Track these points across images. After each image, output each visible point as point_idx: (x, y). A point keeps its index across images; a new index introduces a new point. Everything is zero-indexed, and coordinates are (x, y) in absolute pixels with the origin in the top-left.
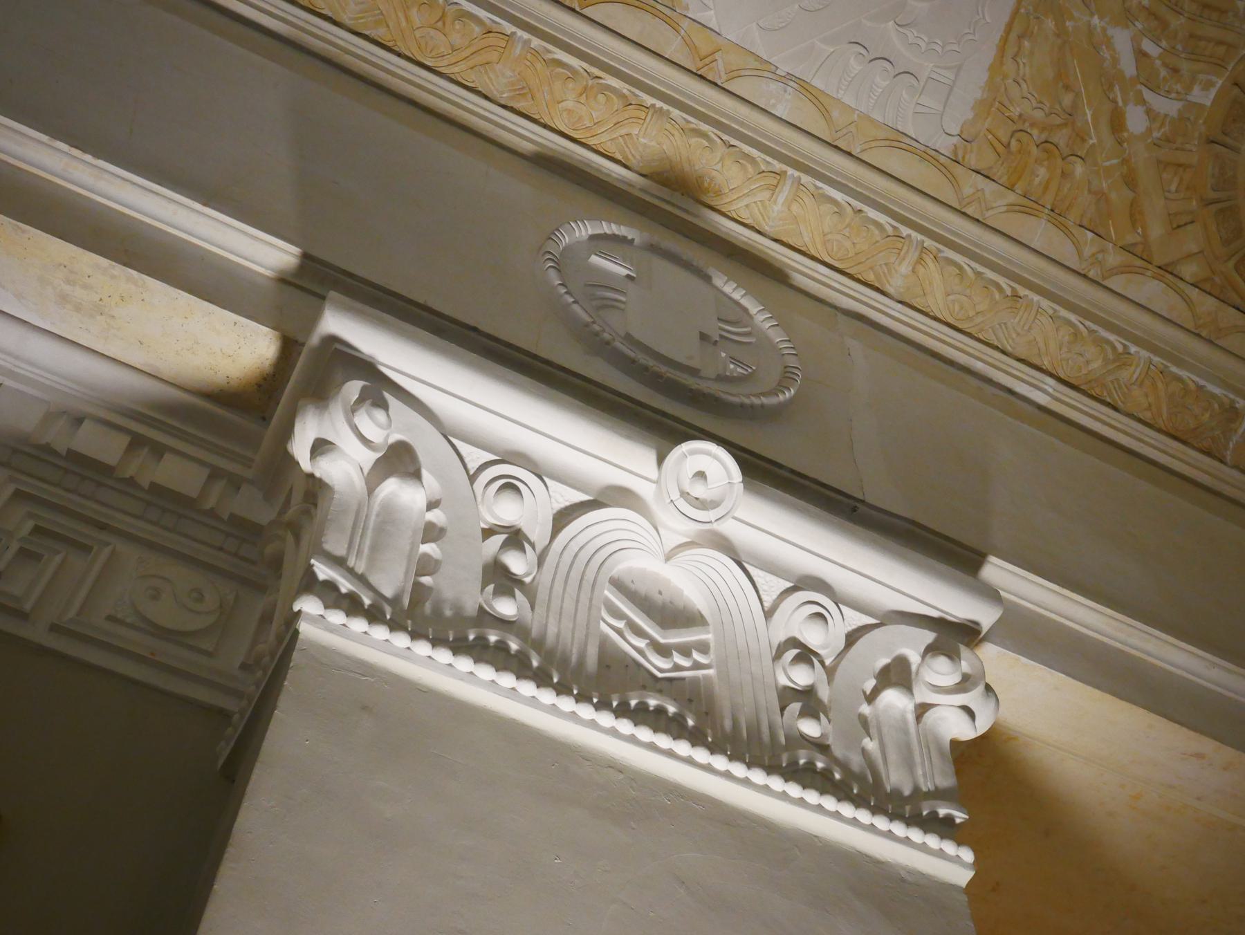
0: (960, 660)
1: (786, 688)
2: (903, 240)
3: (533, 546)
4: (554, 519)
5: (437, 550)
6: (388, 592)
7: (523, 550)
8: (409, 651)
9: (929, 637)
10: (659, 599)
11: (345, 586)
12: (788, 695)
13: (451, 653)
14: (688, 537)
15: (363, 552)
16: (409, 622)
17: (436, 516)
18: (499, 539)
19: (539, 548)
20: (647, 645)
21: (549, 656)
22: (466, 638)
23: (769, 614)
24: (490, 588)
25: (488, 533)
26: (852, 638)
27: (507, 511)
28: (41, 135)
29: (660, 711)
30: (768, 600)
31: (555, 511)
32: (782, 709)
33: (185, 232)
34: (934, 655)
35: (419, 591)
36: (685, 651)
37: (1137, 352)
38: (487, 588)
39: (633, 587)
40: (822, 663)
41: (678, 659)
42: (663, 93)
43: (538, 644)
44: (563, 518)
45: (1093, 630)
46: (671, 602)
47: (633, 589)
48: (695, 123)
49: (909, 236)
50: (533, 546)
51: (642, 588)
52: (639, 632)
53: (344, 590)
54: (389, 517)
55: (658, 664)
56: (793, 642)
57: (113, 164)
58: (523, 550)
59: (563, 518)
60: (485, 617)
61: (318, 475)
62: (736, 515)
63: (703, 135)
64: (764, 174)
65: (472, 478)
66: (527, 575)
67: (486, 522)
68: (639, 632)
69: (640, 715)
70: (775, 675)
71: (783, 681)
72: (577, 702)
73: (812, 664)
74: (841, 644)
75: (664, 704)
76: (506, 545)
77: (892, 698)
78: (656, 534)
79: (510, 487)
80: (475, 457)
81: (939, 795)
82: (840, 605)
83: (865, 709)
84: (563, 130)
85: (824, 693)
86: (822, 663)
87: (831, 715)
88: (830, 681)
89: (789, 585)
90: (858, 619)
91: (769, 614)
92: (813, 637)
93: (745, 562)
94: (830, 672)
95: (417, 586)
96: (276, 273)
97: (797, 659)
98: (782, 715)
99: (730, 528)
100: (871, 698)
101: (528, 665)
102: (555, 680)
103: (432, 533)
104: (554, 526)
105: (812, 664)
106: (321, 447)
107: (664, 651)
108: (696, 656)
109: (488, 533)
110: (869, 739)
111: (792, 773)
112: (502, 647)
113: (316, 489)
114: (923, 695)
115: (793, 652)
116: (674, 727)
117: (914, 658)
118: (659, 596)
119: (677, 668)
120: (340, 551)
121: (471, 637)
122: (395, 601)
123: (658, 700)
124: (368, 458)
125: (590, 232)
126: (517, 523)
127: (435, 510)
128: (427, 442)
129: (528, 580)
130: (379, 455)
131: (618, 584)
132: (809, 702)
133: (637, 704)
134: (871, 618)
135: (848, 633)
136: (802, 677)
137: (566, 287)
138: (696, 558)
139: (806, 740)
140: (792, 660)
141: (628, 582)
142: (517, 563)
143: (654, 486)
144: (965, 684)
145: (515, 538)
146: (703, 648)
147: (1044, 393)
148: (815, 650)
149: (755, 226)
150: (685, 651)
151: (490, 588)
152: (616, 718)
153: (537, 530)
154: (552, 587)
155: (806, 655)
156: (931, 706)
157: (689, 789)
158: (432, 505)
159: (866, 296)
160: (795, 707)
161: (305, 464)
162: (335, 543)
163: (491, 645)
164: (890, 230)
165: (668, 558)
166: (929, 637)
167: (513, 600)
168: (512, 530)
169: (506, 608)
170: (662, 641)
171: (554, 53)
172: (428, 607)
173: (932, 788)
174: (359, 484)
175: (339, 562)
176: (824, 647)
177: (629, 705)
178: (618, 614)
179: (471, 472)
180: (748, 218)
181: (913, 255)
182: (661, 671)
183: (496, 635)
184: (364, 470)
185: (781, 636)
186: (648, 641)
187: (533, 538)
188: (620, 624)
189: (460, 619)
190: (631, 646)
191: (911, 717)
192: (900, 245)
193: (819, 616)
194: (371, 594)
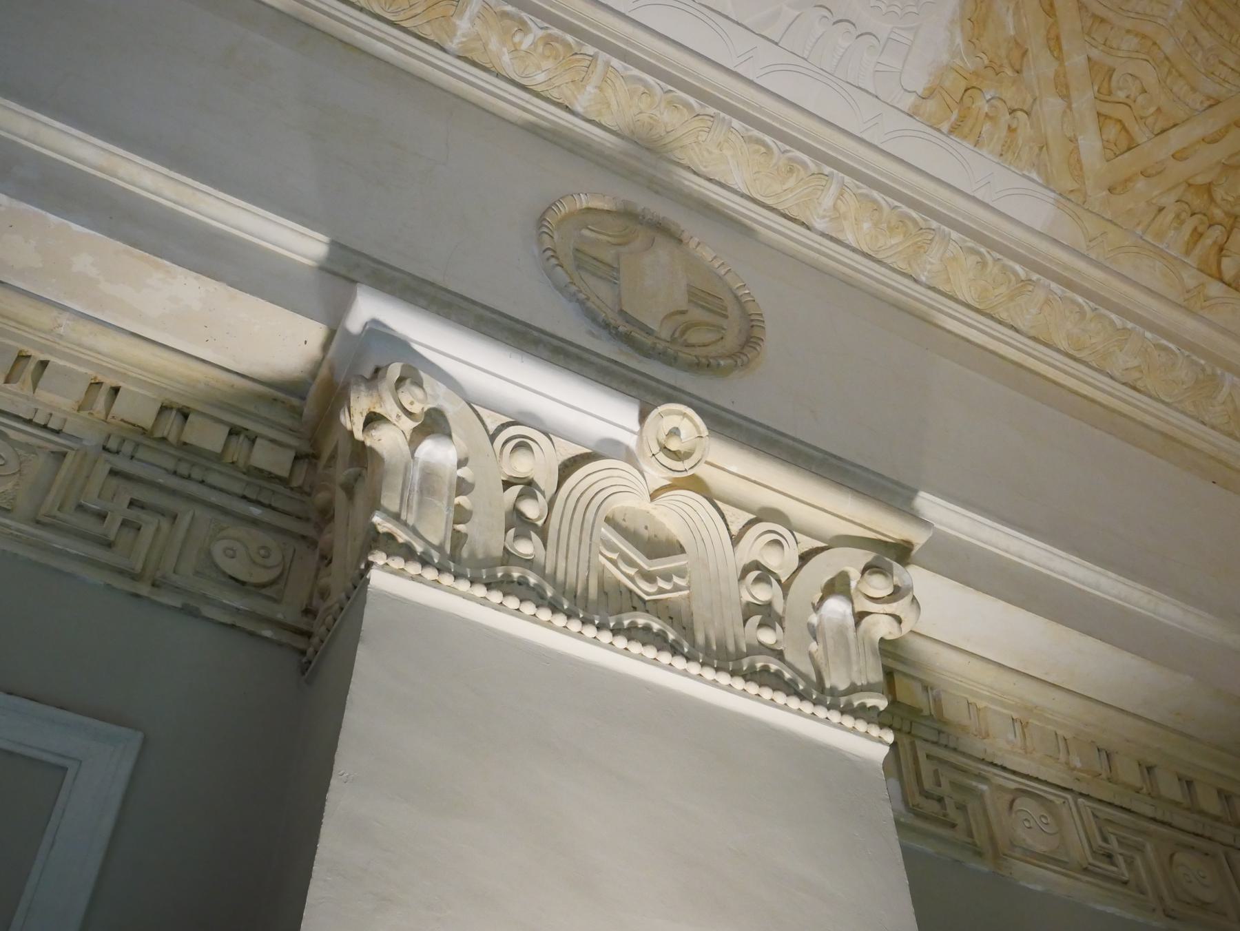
0: (893, 577)
1: (748, 604)
2: (827, 178)
3: (543, 493)
4: (559, 470)
5: (468, 501)
6: (436, 542)
7: (535, 498)
8: (566, 629)
9: (866, 556)
10: (646, 534)
11: (402, 536)
12: (749, 610)
13: (729, 676)
14: (670, 480)
15: (412, 507)
16: (716, 661)
17: (464, 472)
18: (516, 490)
19: (549, 493)
20: (637, 572)
21: (562, 589)
22: (495, 576)
23: (735, 540)
24: (512, 532)
25: (507, 484)
26: (805, 558)
27: (522, 466)
28: (267, 212)
29: (765, 669)
30: (735, 529)
31: (560, 462)
32: (745, 622)
33: (223, 223)
34: (871, 574)
35: (458, 539)
36: (667, 577)
37: (1039, 280)
38: (510, 531)
39: (624, 524)
40: (779, 581)
41: (662, 584)
42: (584, 23)
43: (552, 579)
44: (568, 468)
45: (281, 225)
46: (656, 536)
47: (624, 527)
48: (756, 133)
49: (832, 173)
50: (543, 493)
51: (629, 524)
52: (631, 563)
53: (401, 540)
54: (429, 475)
55: (644, 589)
56: (756, 565)
57: (270, 211)
58: (535, 498)
59: (568, 468)
60: (508, 557)
61: (368, 443)
62: (709, 459)
63: (765, 144)
64: (700, 117)
65: (492, 438)
66: (539, 518)
67: (505, 474)
68: (631, 563)
69: (632, 633)
70: (740, 592)
71: (746, 598)
72: (732, 676)
73: (770, 583)
74: (795, 563)
75: (782, 670)
76: (521, 496)
77: (836, 607)
78: (643, 479)
79: (523, 445)
80: (493, 421)
81: (869, 688)
82: (795, 533)
83: (814, 619)
84: (513, 77)
85: (779, 607)
86: (779, 581)
87: (786, 624)
88: (785, 595)
89: (752, 516)
90: (808, 544)
91: (735, 540)
92: (772, 560)
93: (551, 434)
94: (785, 587)
95: (455, 532)
96: (316, 261)
97: (758, 580)
98: (744, 625)
99: (703, 471)
100: (817, 608)
101: (665, 639)
102: (814, 697)
103: (463, 487)
104: (560, 475)
105: (770, 583)
106: (373, 420)
107: (649, 577)
108: (676, 579)
109: (507, 484)
110: (815, 643)
111: (750, 675)
112: (522, 582)
113: (363, 455)
114: (863, 605)
115: (753, 575)
116: (660, 641)
117: (855, 574)
118: (646, 531)
119: (662, 591)
120: (394, 507)
121: (500, 575)
122: (440, 548)
123: (645, 618)
124: (408, 425)
125: (585, 205)
126: (529, 475)
127: (463, 468)
128: (453, 409)
129: (540, 523)
130: (416, 424)
131: (609, 521)
132: (768, 615)
133: (629, 624)
134: (818, 542)
135: (802, 554)
136: (762, 594)
137: (557, 258)
138: (673, 498)
139: (767, 647)
140: (753, 581)
141: (619, 519)
142: (531, 509)
143: (635, 437)
144: (897, 593)
145: (529, 487)
146: (681, 573)
147: (1010, 348)
148: (774, 571)
149: (691, 166)
150: (667, 577)
151: (512, 532)
152: (881, 729)
153: (546, 479)
154: (559, 530)
155: (765, 575)
156: (869, 613)
157: (836, 748)
158: (462, 463)
159: (831, 250)
160: (756, 619)
161: (359, 435)
162: (390, 501)
163: (640, 626)
164: (922, 224)
165: (653, 496)
166: (866, 556)
167: (530, 542)
168: (526, 481)
169: (525, 548)
170: (646, 567)
171: (632, 70)
172: (465, 553)
173: (865, 682)
174: (406, 448)
175: (396, 517)
176: (781, 567)
177: (623, 624)
178: (613, 548)
179: (491, 433)
180: (431, 35)
181: (833, 189)
182: (648, 594)
183: (519, 572)
184: (406, 434)
185: (746, 560)
186: (637, 570)
187: (542, 487)
188: (614, 556)
189: (491, 563)
190: (621, 575)
191: (851, 621)
192: (824, 183)
193: (777, 543)
194: (422, 542)
